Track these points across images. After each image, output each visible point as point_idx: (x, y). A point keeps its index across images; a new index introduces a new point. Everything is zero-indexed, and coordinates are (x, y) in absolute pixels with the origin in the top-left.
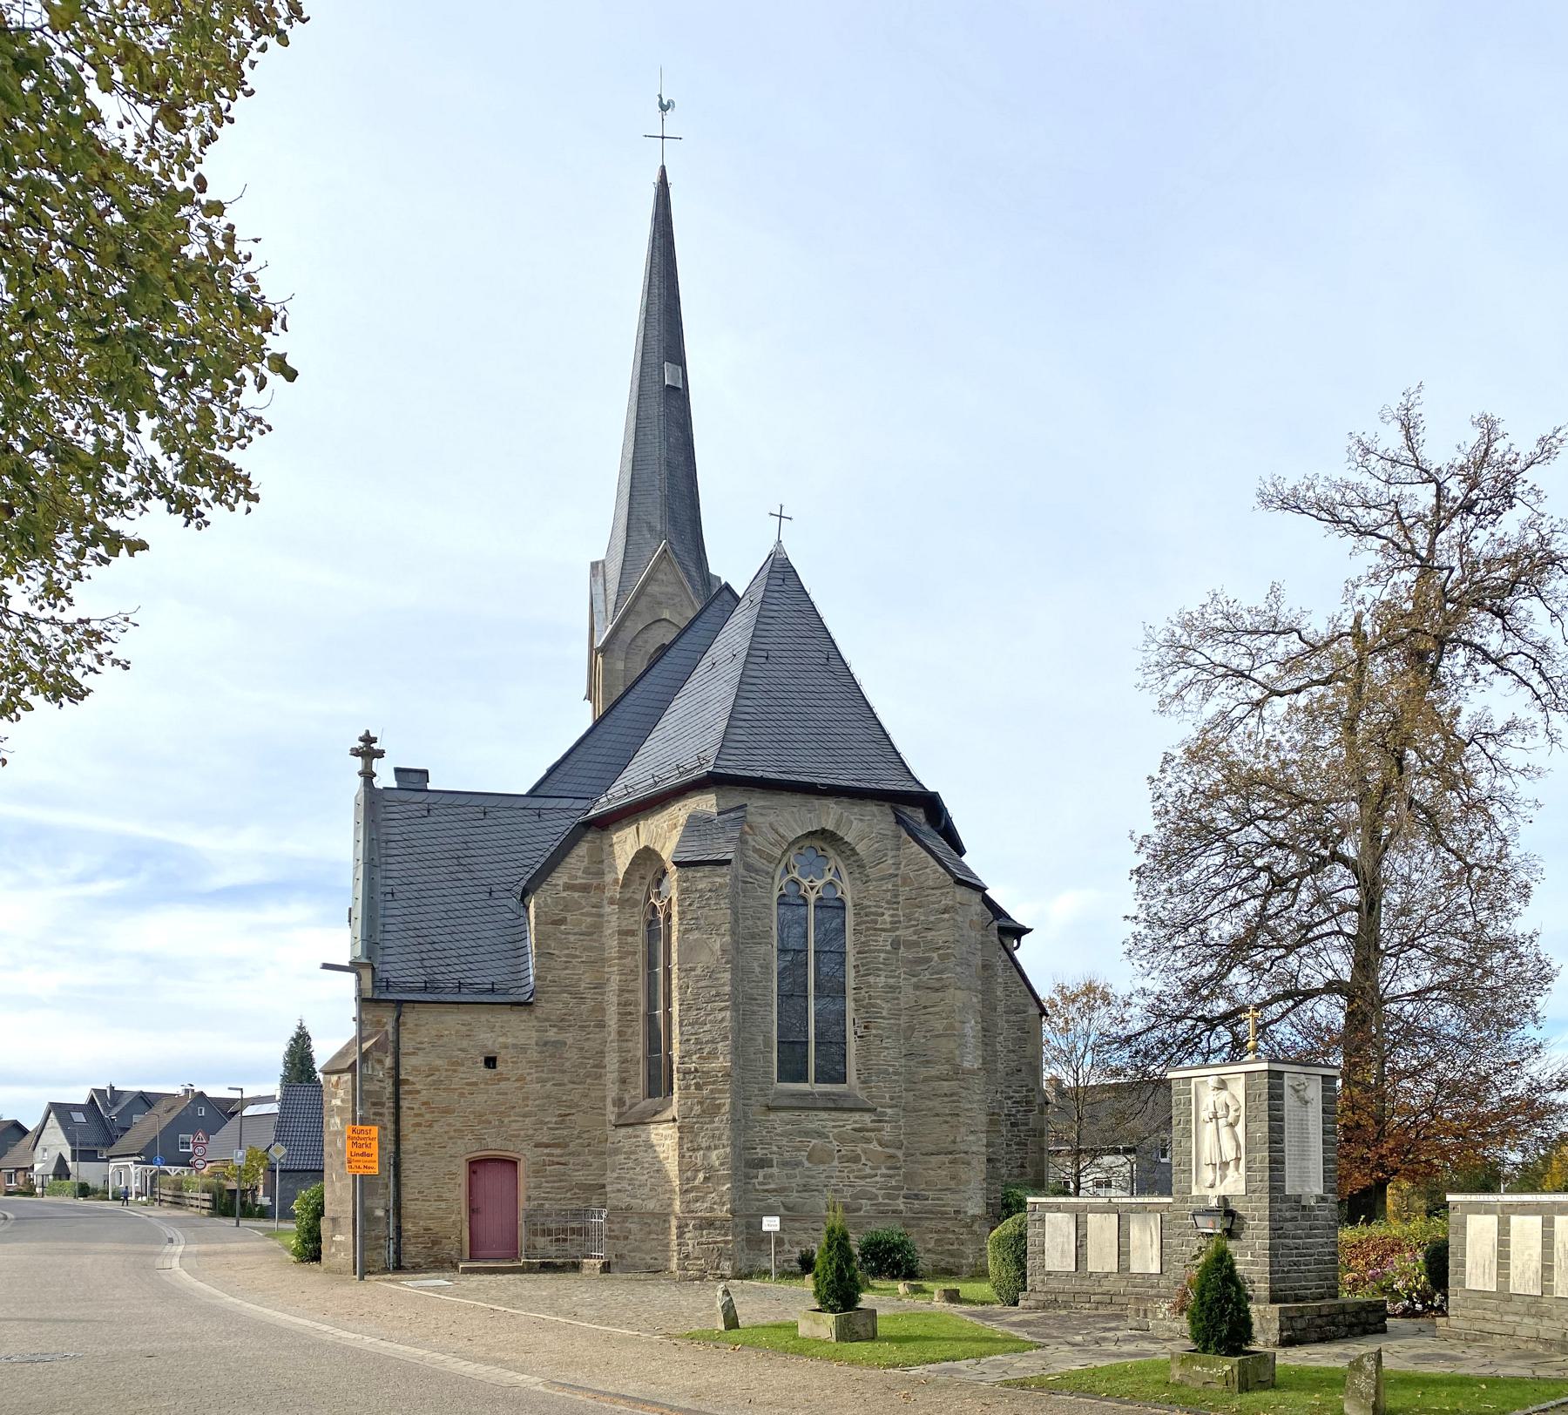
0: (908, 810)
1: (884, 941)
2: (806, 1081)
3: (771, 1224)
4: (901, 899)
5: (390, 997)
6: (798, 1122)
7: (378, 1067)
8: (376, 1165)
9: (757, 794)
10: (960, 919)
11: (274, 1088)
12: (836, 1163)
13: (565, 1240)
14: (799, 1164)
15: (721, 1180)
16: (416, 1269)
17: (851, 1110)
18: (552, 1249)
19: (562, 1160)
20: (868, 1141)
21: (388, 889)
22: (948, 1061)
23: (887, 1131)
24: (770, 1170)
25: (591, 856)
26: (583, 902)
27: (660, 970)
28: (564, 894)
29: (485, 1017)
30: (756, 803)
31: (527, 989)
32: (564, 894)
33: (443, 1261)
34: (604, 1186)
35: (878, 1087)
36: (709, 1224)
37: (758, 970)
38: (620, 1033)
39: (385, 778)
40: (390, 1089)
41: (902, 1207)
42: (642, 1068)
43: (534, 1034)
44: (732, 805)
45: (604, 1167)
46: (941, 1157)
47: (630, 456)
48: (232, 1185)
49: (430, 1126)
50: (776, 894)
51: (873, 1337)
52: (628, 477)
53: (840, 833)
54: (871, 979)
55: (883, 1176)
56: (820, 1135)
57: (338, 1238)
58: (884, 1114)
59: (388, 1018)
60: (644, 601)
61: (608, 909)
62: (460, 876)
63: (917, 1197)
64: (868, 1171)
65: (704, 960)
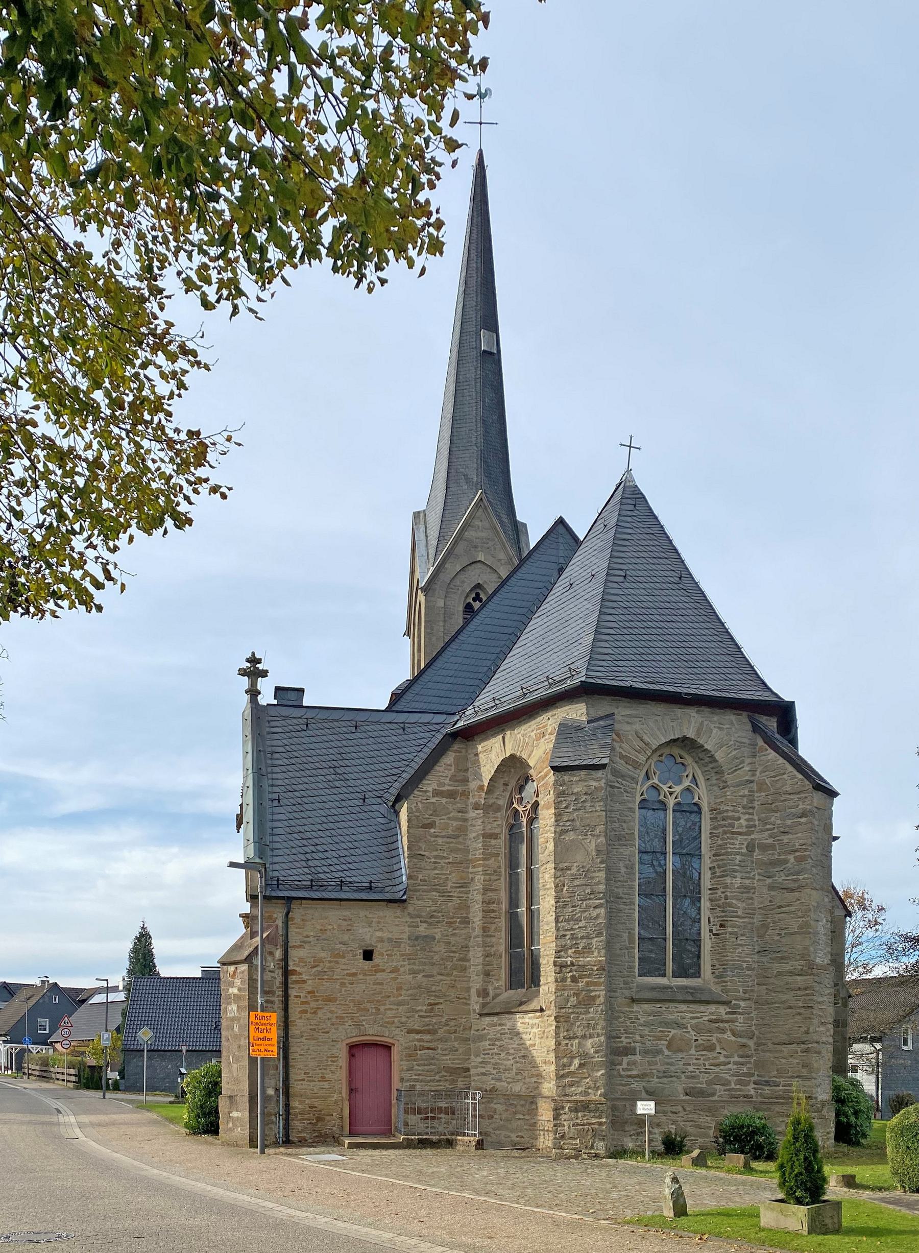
0: (764, 719)
1: (739, 844)
2: (664, 975)
3: (645, 1108)
4: (756, 804)
5: (281, 894)
6: (658, 1014)
7: (269, 958)
8: (275, 1049)
9: (625, 702)
10: (816, 823)
11: (118, 979)
12: (693, 1051)
13: (433, 1118)
14: (659, 1052)
15: (595, 1067)
16: (303, 1143)
17: (708, 1003)
18: (422, 1126)
19: (431, 1045)
20: (723, 1031)
21: (276, 796)
22: (803, 956)
23: (740, 1023)
24: (633, 1057)
25: (457, 765)
26: (450, 807)
27: (522, 870)
28: (434, 800)
29: (362, 912)
30: (623, 711)
31: (401, 887)
32: (434, 800)
33: (326, 1136)
34: (468, 1070)
35: (731, 981)
36: (582, 1107)
37: (623, 870)
38: (485, 929)
39: (267, 697)
40: (279, 978)
41: (752, 1092)
42: (504, 962)
43: (407, 929)
44: (601, 713)
45: (468, 1052)
46: (793, 1047)
47: (450, 416)
48: (91, 1061)
49: (315, 1013)
50: (638, 799)
51: (837, 1231)
52: (447, 435)
53: (701, 741)
54: (728, 880)
55: (736, 1063)
56: (679, 1025)
57: (235, 1114)
58: (739, 1007)
59: (278, 914)
60: (462, 546)
61: (472, 814)
62: (336, 784)
63: (767, 1083)
64: (722, 1059)
65: (579, 860)
